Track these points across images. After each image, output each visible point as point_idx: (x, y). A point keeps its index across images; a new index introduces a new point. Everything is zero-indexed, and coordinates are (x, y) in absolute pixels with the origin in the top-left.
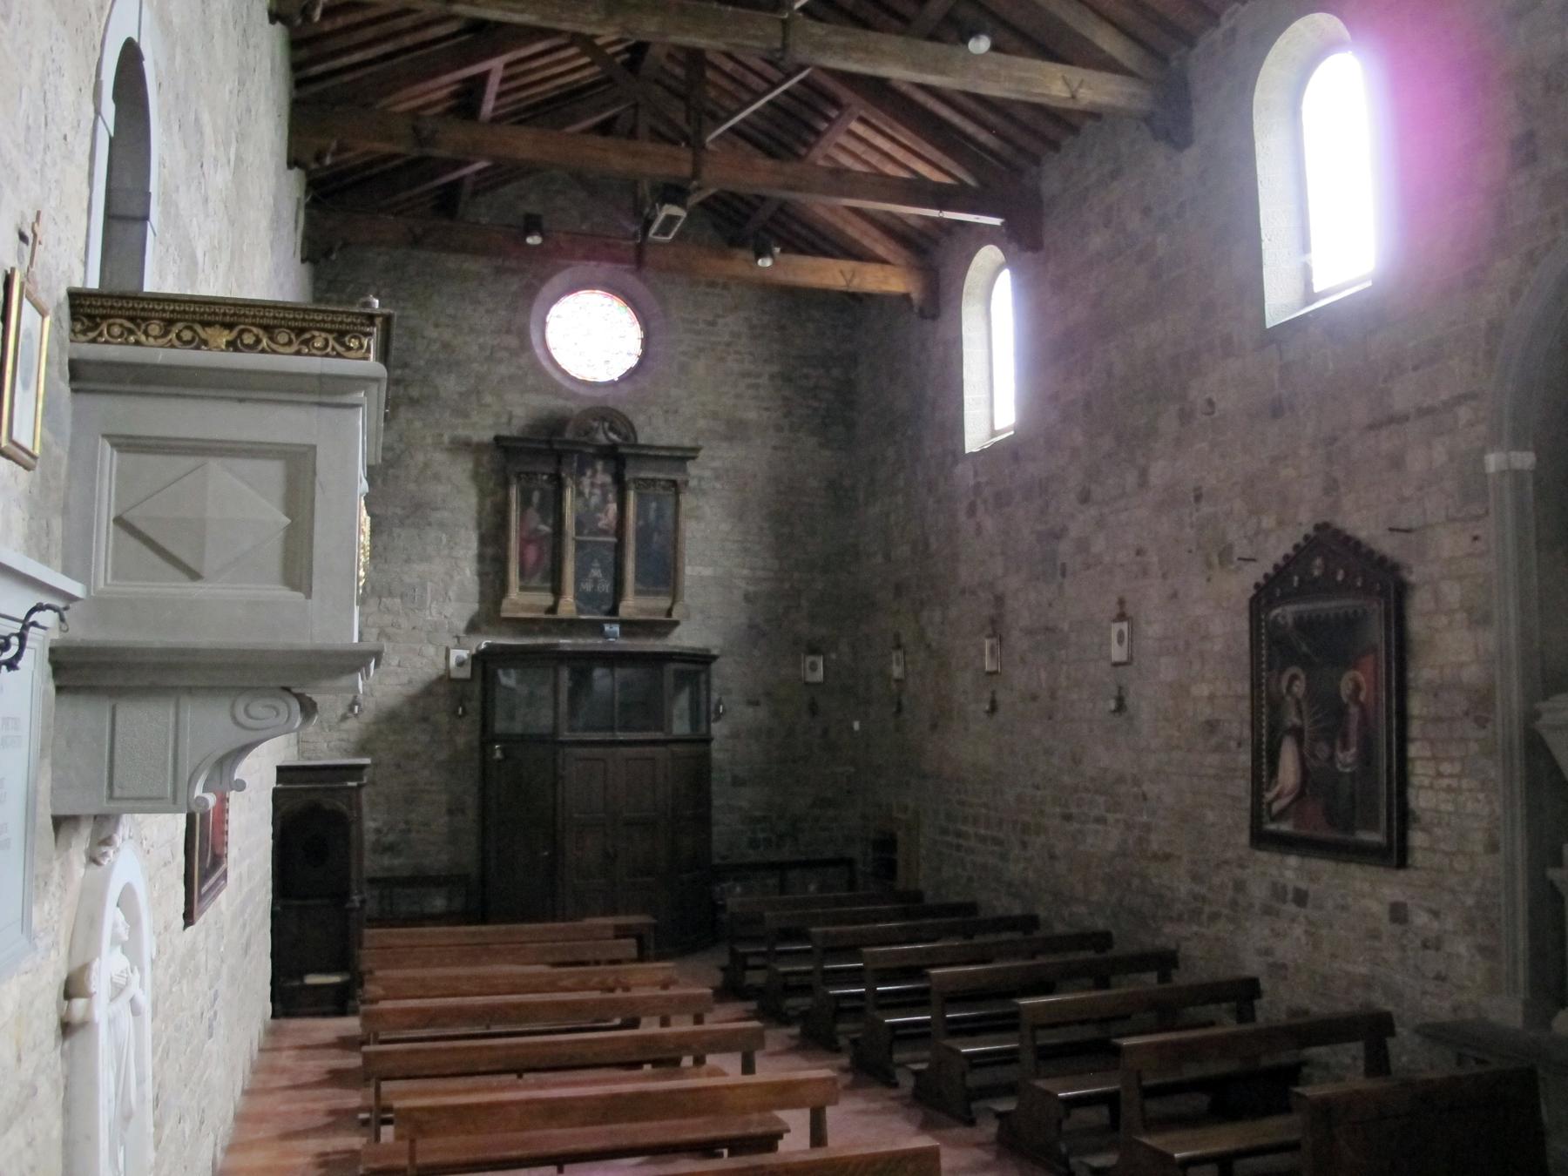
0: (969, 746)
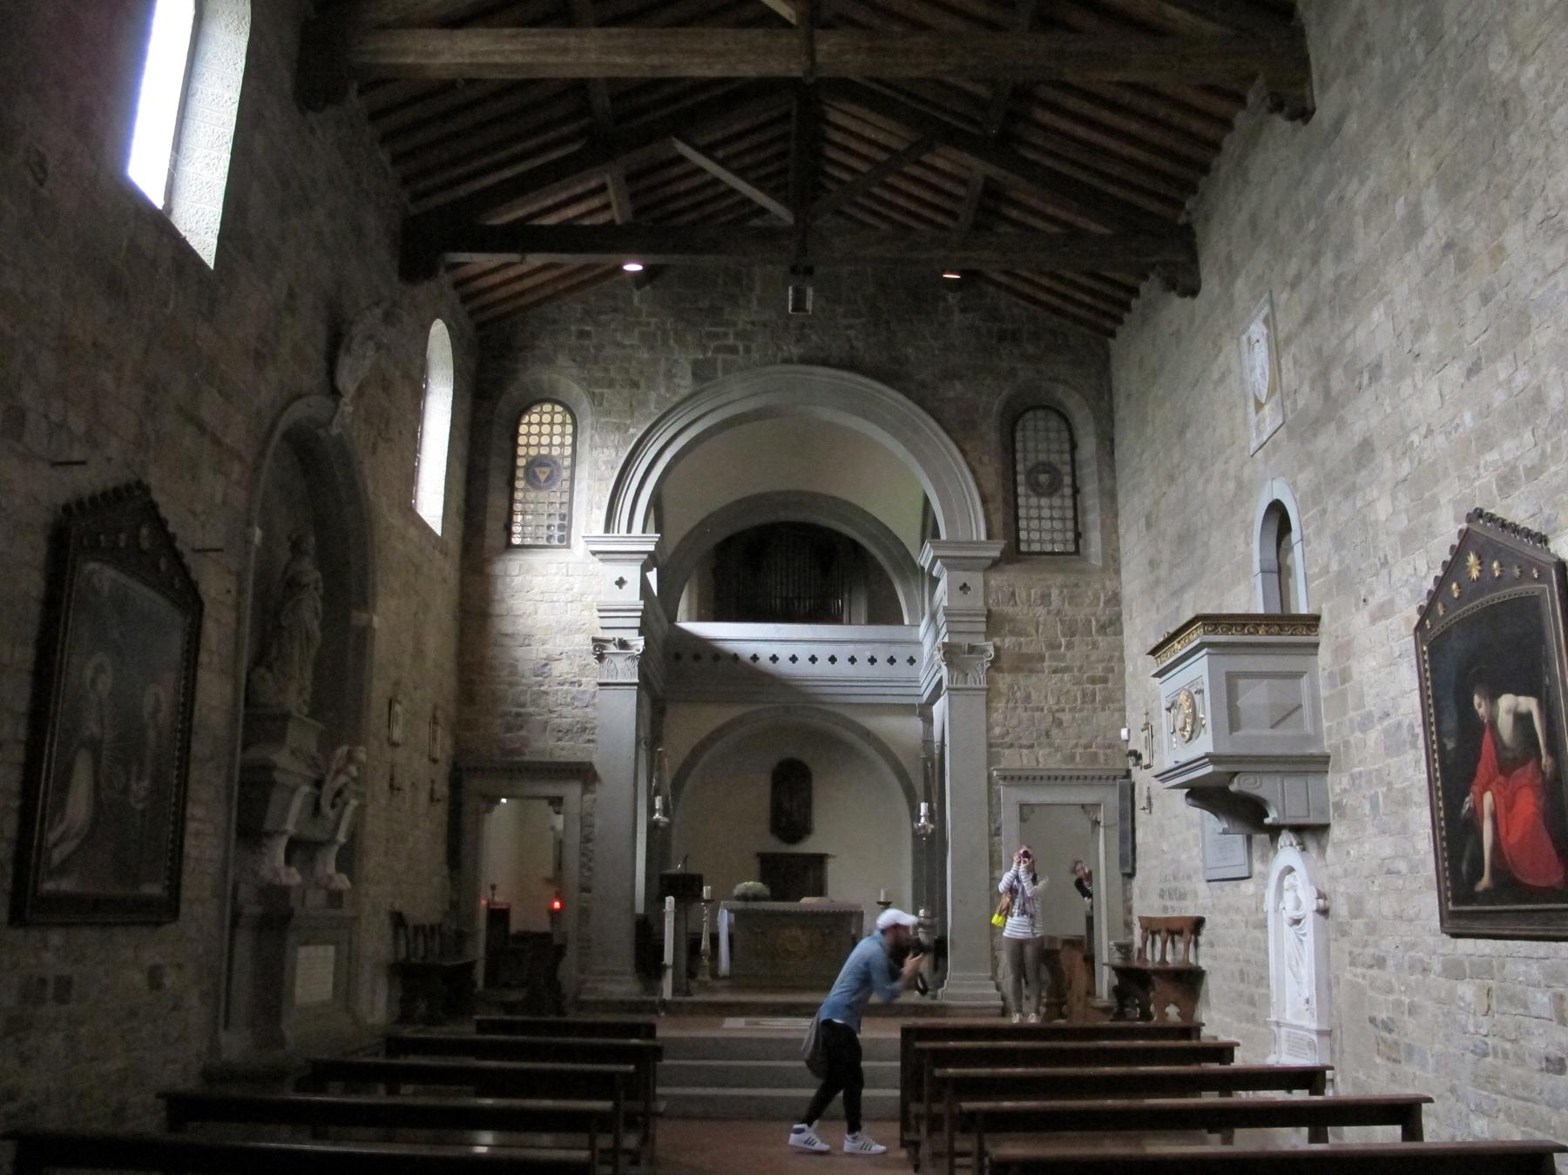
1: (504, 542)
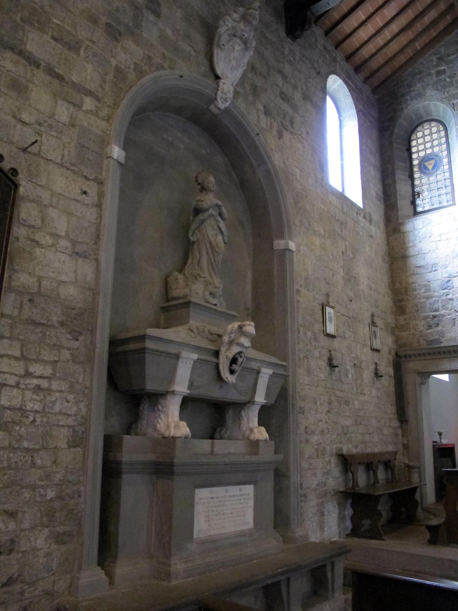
0: (383, 206)
1: (412, 212)
